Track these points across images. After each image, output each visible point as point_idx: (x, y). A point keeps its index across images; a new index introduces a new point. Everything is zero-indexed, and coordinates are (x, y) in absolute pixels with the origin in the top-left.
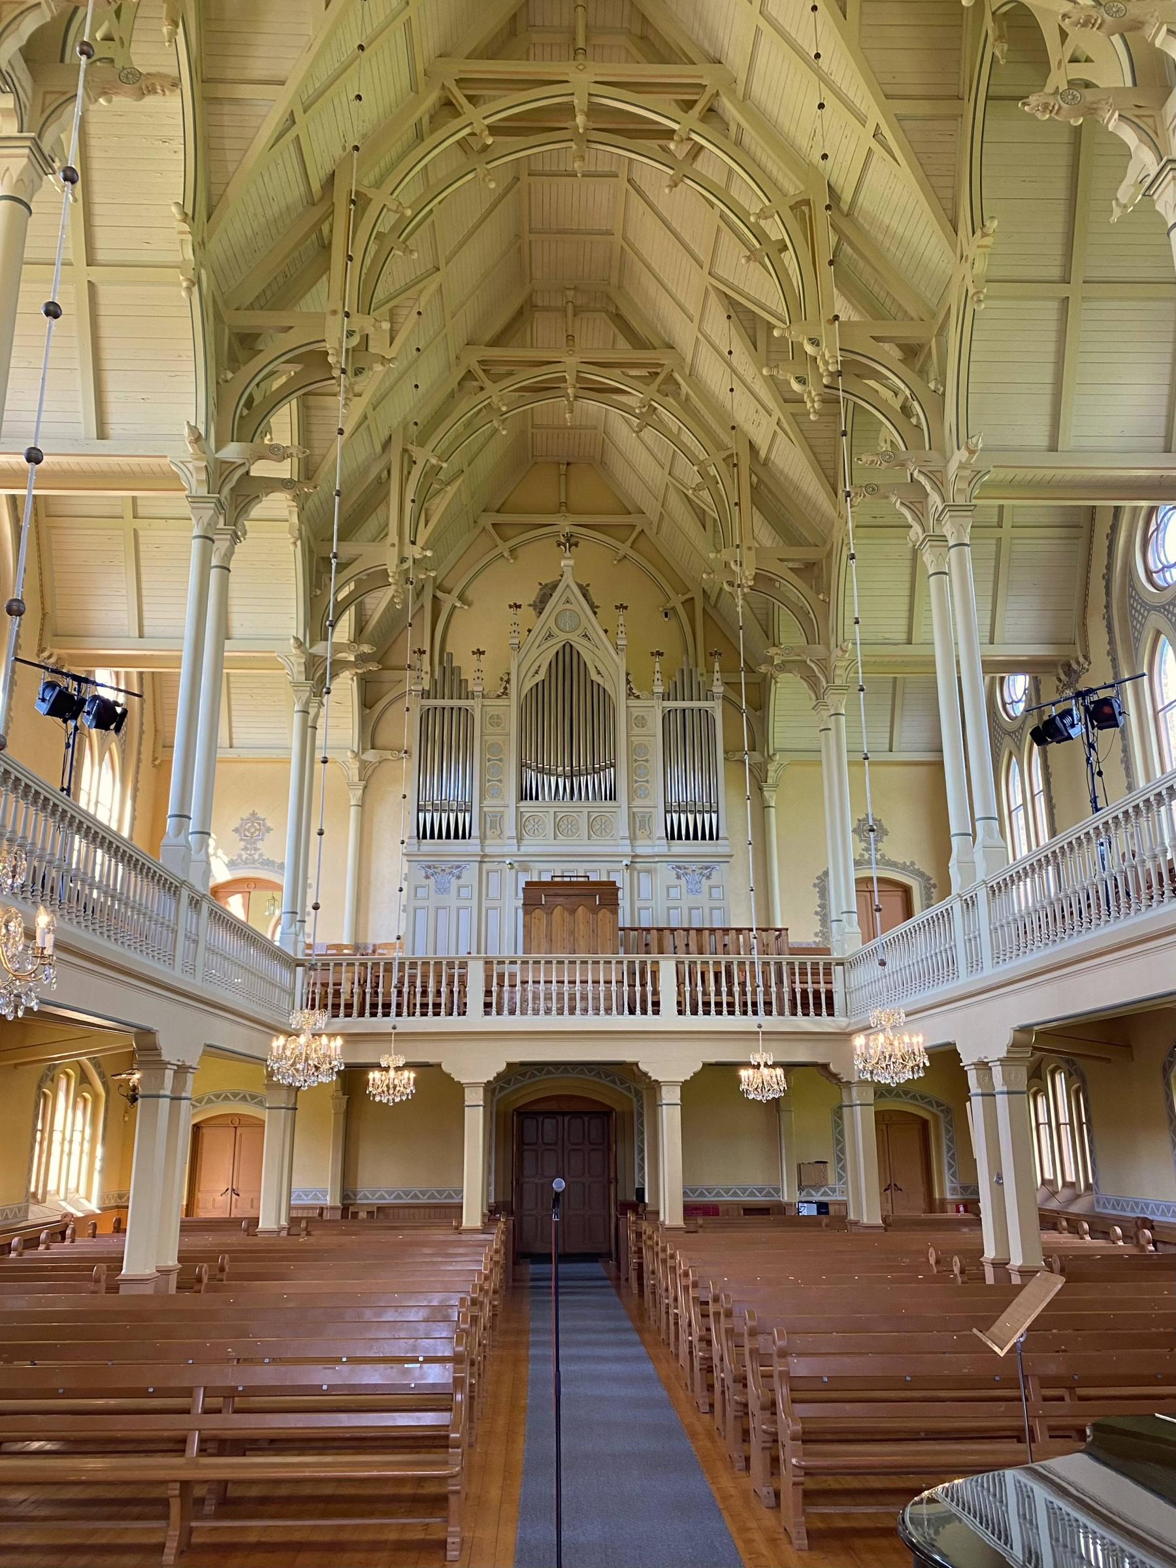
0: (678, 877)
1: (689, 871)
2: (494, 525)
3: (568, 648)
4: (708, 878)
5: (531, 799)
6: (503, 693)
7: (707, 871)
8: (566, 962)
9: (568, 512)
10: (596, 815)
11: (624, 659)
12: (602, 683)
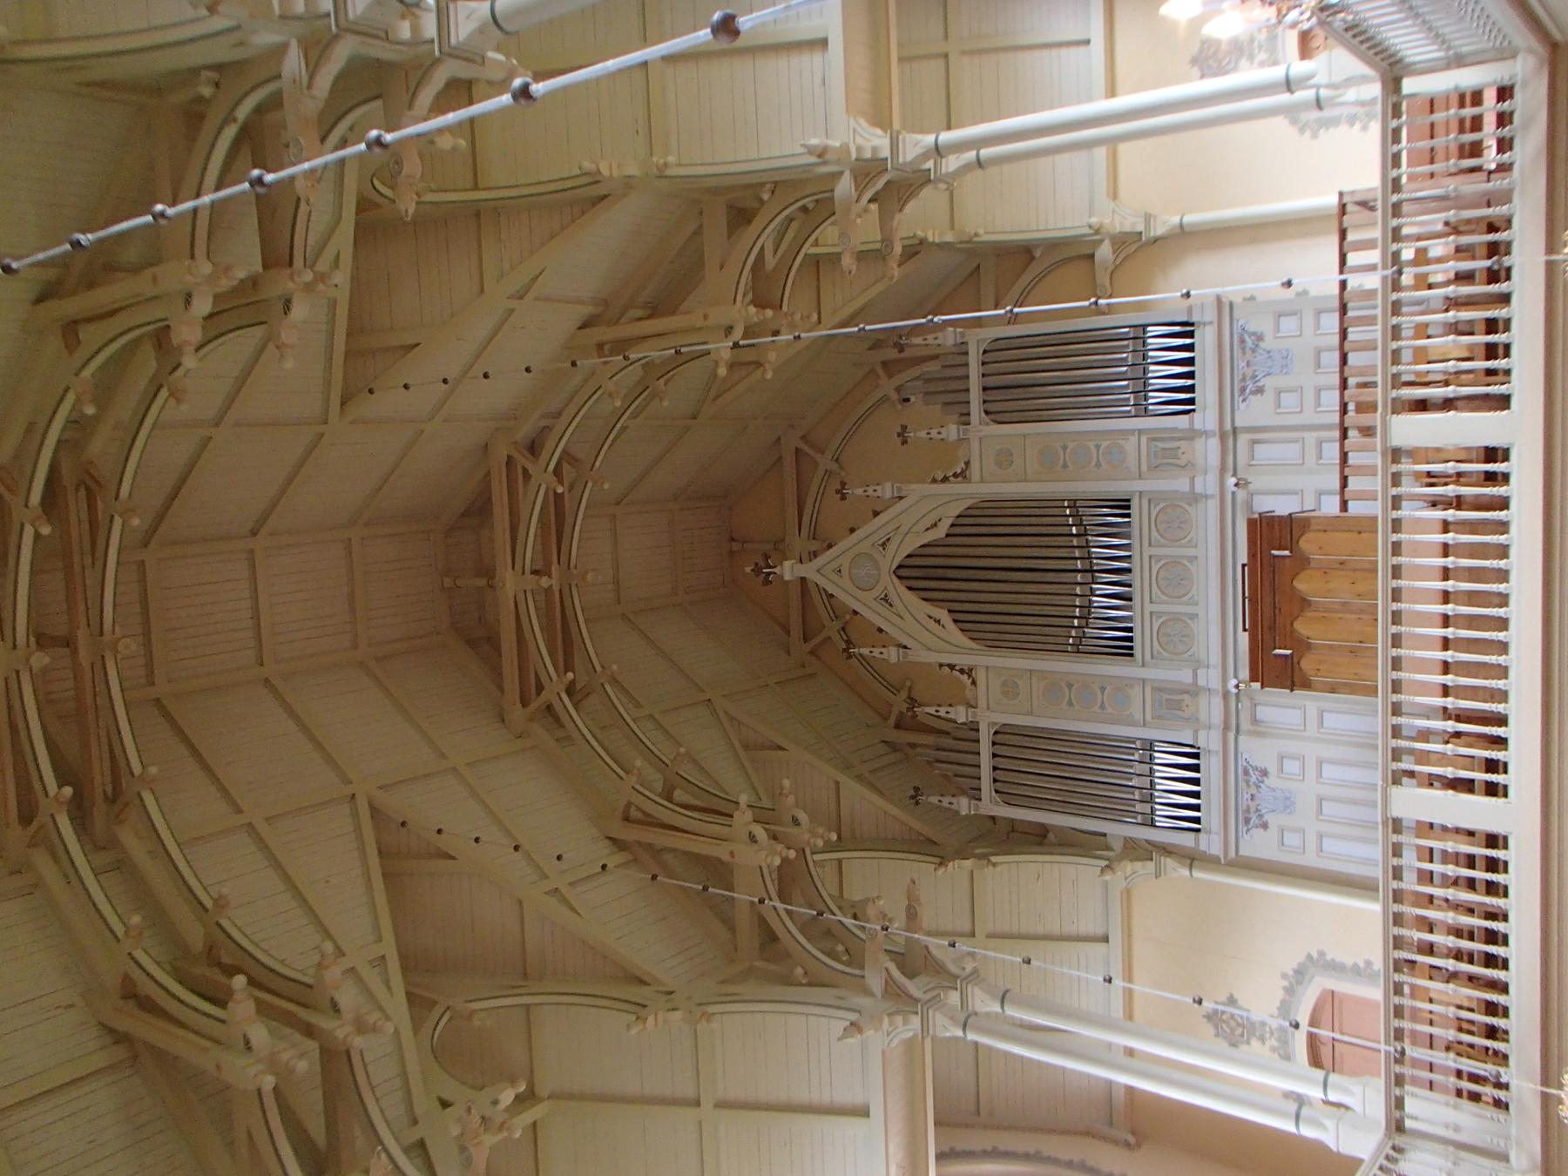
0: (1260, 391)
1: (1249, 372)
2: (806, 640)
3: (902, 572)
4: (1260, 338)
5: (1130, 639)
6: (970, 676)
7: (1249, 342)
8: (1394, 629)
9: (783, 540)
10: (1155, 534)
11: (913, 486)
12: (950, 521)
